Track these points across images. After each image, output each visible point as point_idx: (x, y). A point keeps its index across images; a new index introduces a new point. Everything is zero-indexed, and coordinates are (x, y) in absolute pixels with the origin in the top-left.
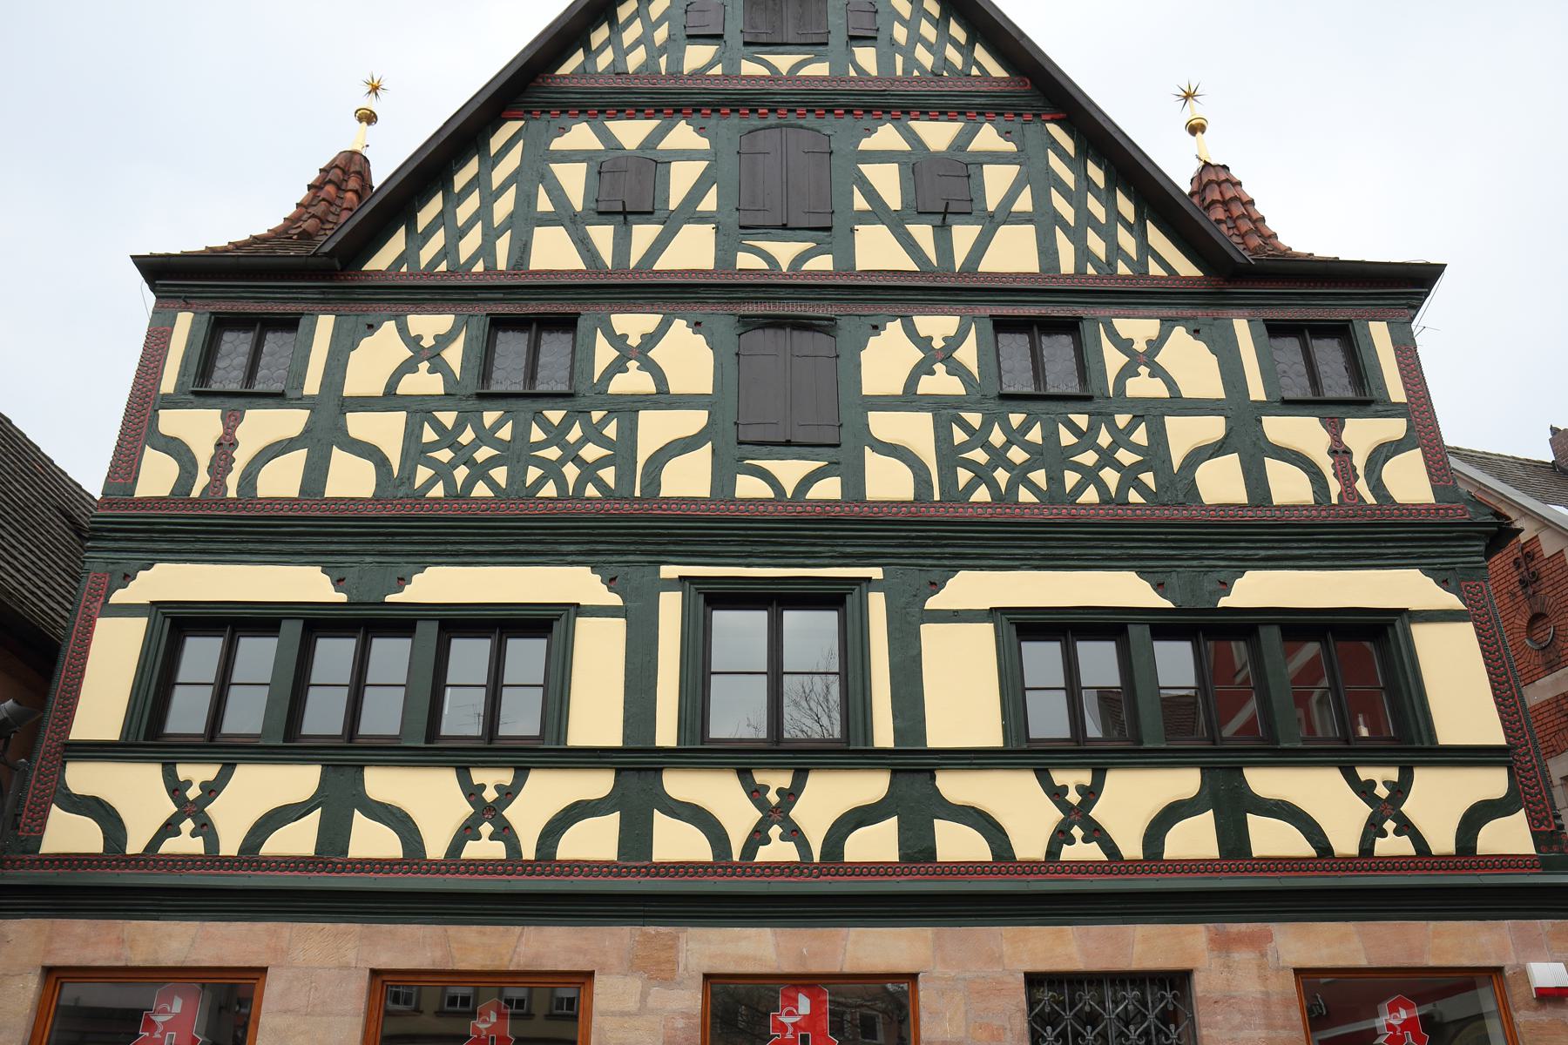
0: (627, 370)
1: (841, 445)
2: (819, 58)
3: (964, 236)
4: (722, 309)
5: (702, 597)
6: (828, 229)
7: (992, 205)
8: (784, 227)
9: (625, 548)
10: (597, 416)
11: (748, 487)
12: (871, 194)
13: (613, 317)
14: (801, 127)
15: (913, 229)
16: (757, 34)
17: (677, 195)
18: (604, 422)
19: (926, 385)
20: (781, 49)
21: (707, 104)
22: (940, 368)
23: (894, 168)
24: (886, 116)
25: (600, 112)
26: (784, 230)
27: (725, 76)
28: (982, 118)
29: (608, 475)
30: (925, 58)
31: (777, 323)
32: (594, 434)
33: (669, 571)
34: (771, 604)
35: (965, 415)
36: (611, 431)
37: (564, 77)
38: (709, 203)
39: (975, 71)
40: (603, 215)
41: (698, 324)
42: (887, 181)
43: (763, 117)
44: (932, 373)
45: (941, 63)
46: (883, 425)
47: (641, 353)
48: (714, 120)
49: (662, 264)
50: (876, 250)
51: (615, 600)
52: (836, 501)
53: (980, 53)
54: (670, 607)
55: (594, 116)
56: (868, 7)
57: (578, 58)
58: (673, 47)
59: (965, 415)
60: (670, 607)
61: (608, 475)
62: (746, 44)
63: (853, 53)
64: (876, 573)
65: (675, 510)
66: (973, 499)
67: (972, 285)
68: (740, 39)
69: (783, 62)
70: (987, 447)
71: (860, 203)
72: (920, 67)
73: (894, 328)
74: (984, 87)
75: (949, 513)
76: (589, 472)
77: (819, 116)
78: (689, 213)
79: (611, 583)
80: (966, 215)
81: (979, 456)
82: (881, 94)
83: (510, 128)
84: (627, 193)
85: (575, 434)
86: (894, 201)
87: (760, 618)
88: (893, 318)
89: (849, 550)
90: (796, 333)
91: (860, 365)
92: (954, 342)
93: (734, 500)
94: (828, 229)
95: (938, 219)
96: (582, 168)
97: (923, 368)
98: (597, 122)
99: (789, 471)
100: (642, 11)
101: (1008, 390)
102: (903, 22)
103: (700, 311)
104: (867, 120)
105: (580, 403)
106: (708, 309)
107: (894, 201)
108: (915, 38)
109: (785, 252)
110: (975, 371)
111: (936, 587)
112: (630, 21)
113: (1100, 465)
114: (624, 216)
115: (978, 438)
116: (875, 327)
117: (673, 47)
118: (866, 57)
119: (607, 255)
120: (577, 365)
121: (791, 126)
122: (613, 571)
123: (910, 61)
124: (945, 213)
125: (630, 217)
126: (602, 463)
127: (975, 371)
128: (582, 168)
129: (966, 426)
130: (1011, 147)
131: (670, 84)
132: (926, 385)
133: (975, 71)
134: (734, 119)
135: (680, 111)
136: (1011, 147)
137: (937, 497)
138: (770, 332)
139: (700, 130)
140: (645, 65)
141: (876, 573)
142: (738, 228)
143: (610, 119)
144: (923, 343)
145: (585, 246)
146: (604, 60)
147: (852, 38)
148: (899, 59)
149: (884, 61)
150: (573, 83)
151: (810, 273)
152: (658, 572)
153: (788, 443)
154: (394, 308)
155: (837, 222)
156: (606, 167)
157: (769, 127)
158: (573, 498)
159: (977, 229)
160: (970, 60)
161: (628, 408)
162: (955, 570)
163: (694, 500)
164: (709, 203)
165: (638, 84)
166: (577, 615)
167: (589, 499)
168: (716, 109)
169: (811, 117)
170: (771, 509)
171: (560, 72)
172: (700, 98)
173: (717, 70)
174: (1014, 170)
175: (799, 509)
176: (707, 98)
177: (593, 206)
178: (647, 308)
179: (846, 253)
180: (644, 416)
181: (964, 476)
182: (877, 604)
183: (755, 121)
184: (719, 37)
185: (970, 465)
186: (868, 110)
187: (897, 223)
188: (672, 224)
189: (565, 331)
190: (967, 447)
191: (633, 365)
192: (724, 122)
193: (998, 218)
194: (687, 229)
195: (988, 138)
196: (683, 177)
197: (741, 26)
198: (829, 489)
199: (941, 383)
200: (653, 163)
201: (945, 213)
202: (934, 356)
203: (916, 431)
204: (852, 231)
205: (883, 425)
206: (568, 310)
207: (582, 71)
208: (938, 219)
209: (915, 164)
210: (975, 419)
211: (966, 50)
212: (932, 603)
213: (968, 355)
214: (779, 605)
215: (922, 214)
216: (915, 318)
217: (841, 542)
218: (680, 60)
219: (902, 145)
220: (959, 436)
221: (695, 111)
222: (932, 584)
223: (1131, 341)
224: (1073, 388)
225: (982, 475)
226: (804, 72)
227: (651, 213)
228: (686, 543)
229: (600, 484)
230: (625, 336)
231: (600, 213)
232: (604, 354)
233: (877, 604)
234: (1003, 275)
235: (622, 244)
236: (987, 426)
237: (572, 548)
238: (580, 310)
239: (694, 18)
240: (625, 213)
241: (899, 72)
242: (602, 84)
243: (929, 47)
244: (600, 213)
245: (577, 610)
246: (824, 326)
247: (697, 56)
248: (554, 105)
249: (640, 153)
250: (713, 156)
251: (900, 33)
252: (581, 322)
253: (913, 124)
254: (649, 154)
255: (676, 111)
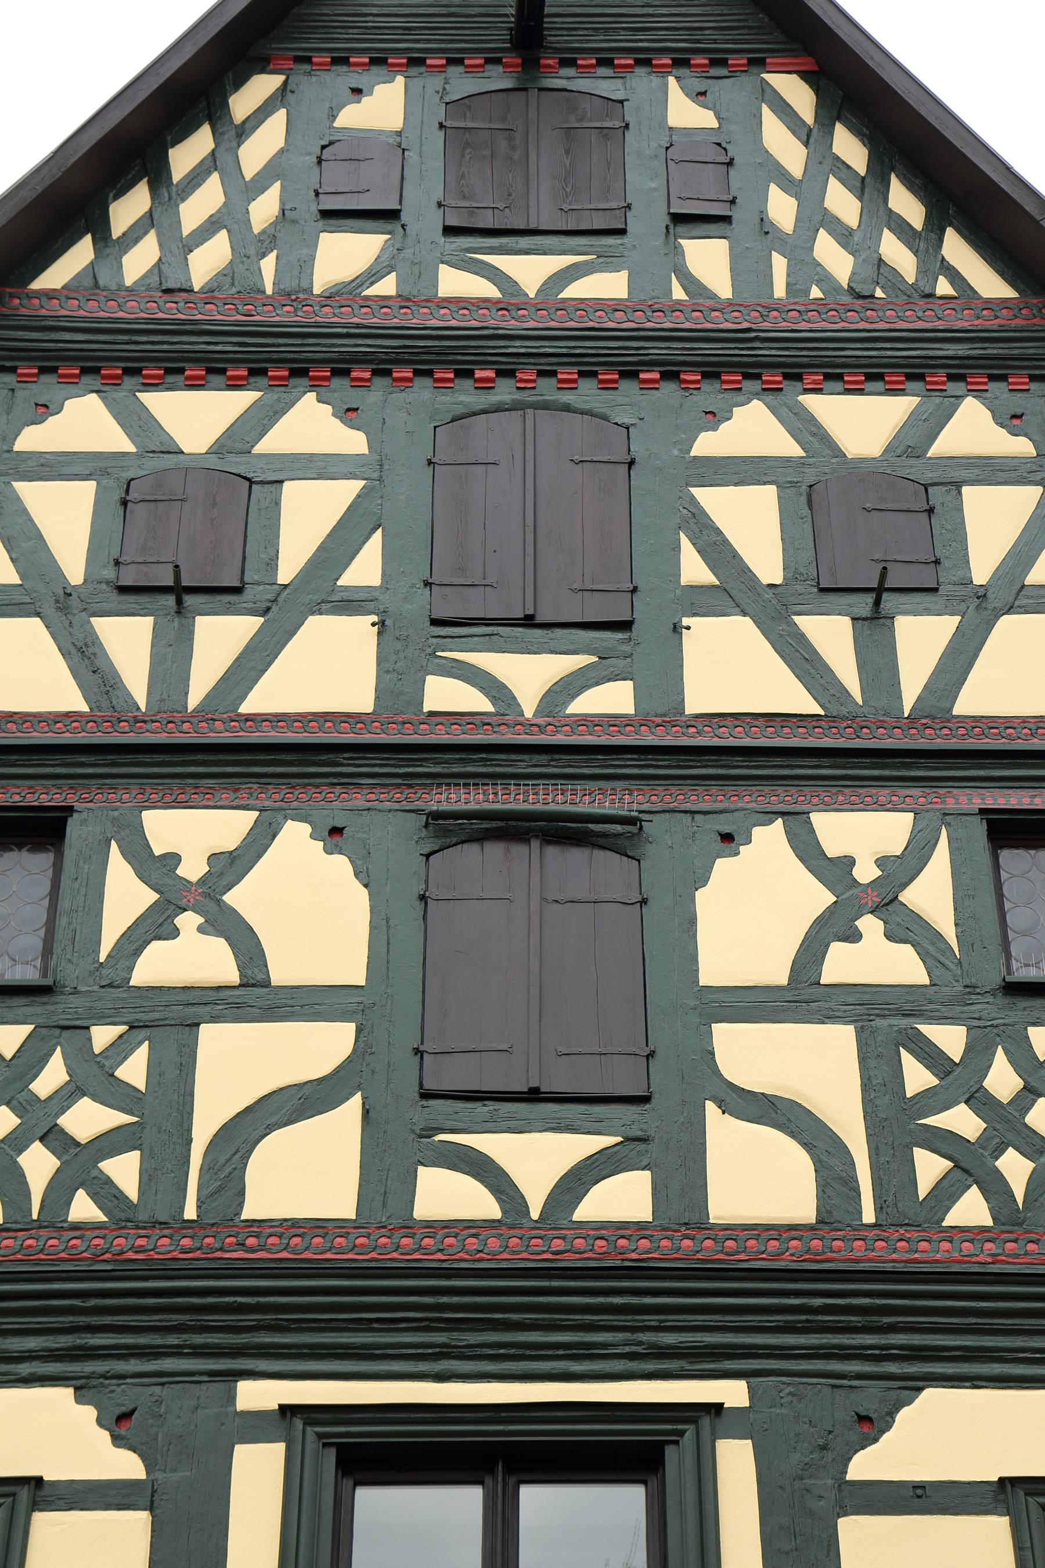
0: (175, 933)
1: (647, 1090)
2: (606, 262)
3: (921, 640)
4: (389, 799)
5: (331, 1455)
6: (625, 626)
7: (981, 573)
8: (529, 621)
9: (156, 1340)
10: (102, 1036)
11: (444, 1195)
12: (717, 549)
13: (146, 815)
14: (567, 408)
15: (807, 624)
16: (472, 211)
17: (292, 559)
18: (120, 1050)
19: (842, 964)
20: (525, 242)
21: (360, 359)
22: (870, 925)
23: (768, 494)
24: (748, 385)
25: (128, 372)
26: (529, 627)
27: (404, 300)
28: (958, 388)
29: (124, 1171)
30: (836, 261)
31: (581, 1253)
32: (94, 1079)
33: (257, 1395)
34: (491, 1470)
35: (929, 1030)
36: (134, 1071)
37: (50, 295)
38: (365, 569)
39: (943, 287)
40: (131, 595)
41: (336, 831)
42: (753, 524)
43: (485, 385)
44: (853, 936)
45: (870, 271)
46: (745, 1053)
47: (208, 896)
48: (376, 395)
49: (258, 701)
50: (730, 672)
51: (128, 1466)
52: (640, 1226)
53: (955, 247)
54: (258, 1475)
55: (115, 381)
56: (713, 154)
57: (80, 255)
58: (291, 235)
59: (929, 1030)
60: (258, 1475)
61: (124, 1171)
62: (449, 231)
63: (679, 251)
64: (733, 1393)
65: (276, 1251)
66: (951, 1219)
67: (939, 744)
68: (435, 221)
69: (530, 270)
70: (980, 1100)
71: (694, 569)
72: (825, 279)
73: (769, 839)
74: (963, 321)
75: (894, 1253)
76: (80, 1163)
77: (607, 386)
78: (321, 591)
79: (120, 1424)
80: (925, 593)
81: (962, 1121)
82: (740, 337)
83: (263, 86)
84: (184, 547)
85: (52, 1076)
86: (767, 564)
87: (463, 1505)
88: (768, 816)
89: (669, 1339)
90: (552, 851)
91: (693, 921)
92: (902, 868)
93: (410, 1226)
94: (623, 626)
95: (864, 604)
96: (82, 494)
97: (834, 927)
98: (119, 394)
99: (537, 1158)
100: (223, 158)
101: (1023, 973)
102: (788, 183)
103: (341, 804)
104: (709, 394)
105: (63, 1007)
106: (359, 799)
107: (767, 564)
108: (815, 217)
109: (529, 674)
110: (949, 933)
111: (871, 1426)
112: (196, 178)
113: (994, 1143)
114: (176, 597)
115: (960, 1081)
116: (727, 838)
117: (291, 235)
118: (709, 260)
119: (135, 674)
120: (63, 921)
121: (546, 406)
122: (127, 1395)
123: (806, 269)
124: (879, 591)
125: (189, 600)
126: (111, 1143)
127: (949, 933)
128: (82, 494)
129: (931, 1056)
130: (1022, 447)
131: (283, 315)
132: (842, 964)
133: (943, 287)
134: (423, 391)
135: (303, 373)
136: (1022, 447)
137: (869, 1216)
138: (494, 850)
139: (348, 414)
140: (227, 274)
141: (733, 1393)
142: (429, 623)
143: (148, 387)
144: (835, 871)
145: (87, 660)
146: (139, 261)
147: (679, 219)
148: (779, 264)
149: (748, 268)
150: (70, 309)
151: (586, 721)
152: (232, 1397)
153: (534, 1096)
154: (783, 797)
155: (643, 611)
156: (136, 489)
157: (498, 409)
158: (40, 1224)
159: (949, 624)
160: (934, 264)
161: (175, 1019)
162: (915, 1385)
163: (319, 1226)
164: (365, 569)
165: (213, 313)
166: (36, 1505)
167: (76, 1227)
168: (382, 368)
169: (587, 386)
170: (494, 1244)
171: (37, 285)
172: (348, 346)
173: (387, 286)
174: (1024, 499)
175: (558, 1244)
176: (363, 346)
177: (109, 573)
178: (227, 796)
179: (664, 677)
180: (212, 1037)
181: (929, 1168)
182: (736, 1462)
183: (465, 395)
184: (392, 215)
185: (943, 1142)
186: (711, 372)
187: (774, 614)
188: (282, 615)
189: (38, 847)
190: (934, 1100)
191: (188, 921)
192: (399, 397)
193: (995, 601)
194: (318, 629)
195: (972, 428)
196: (306, 517)
197: (438, 194)
198: (624, 1198)
199: (874, 959)
200: (243, 484)
201: (879, 591)
202: (858, 900)
203: (818, 1065)
204: (677, 629)
205: (745, 1053)
206: (45, 799)
207: (89, 283)
208: (864, 604)
209: (814, 487)
210: (951, 1039)
211: (925, 243)
212: (863, 1467)
213: (932, 895)
214: (509, 1471)
215: (829, 593)
216: (816, 818)
217: (652, 1319)
218: (307, 264)
219: (784, 445)
220: (917, 1077)
221: (336, 373)
222: (864, 1419)
223: (173, 859)
224: (870, 598)
225: (970, 1165)
226: (575, 290)
227: (237, 590)
228: (300, 1327)
229: (105, 1192)
230: (173, 859)
231: (123, 590)
232: (125, 896)
233: (736, 1462)
234: (1008, 722)
235: (172, 656)
236: (978, 1055)
237: (32, 1343)
238: (71, 800)
239: (336, 176)
240: (179, 591)
241: (780, 291)
242: (133, 311)
243: (844, 236)
244: (123, 590)
245: (34, 1493)
246: (619, 837)
247: (343, 256)
248: (27, 354)
249: (214, 462)
250: (376, 470)
251: (782, 209)
252: (74, 828)
253: (810, 401)
254: (236, 464)
255: (295, 373)
